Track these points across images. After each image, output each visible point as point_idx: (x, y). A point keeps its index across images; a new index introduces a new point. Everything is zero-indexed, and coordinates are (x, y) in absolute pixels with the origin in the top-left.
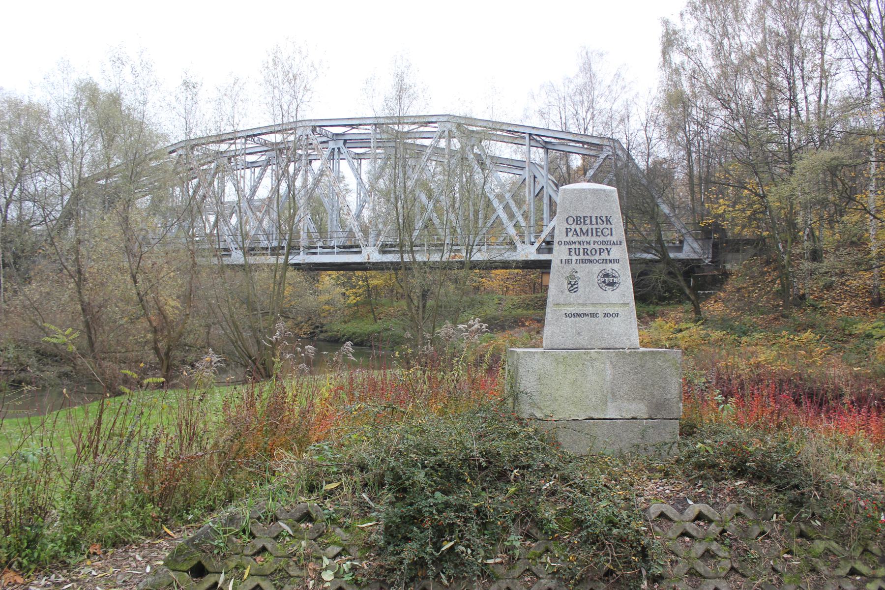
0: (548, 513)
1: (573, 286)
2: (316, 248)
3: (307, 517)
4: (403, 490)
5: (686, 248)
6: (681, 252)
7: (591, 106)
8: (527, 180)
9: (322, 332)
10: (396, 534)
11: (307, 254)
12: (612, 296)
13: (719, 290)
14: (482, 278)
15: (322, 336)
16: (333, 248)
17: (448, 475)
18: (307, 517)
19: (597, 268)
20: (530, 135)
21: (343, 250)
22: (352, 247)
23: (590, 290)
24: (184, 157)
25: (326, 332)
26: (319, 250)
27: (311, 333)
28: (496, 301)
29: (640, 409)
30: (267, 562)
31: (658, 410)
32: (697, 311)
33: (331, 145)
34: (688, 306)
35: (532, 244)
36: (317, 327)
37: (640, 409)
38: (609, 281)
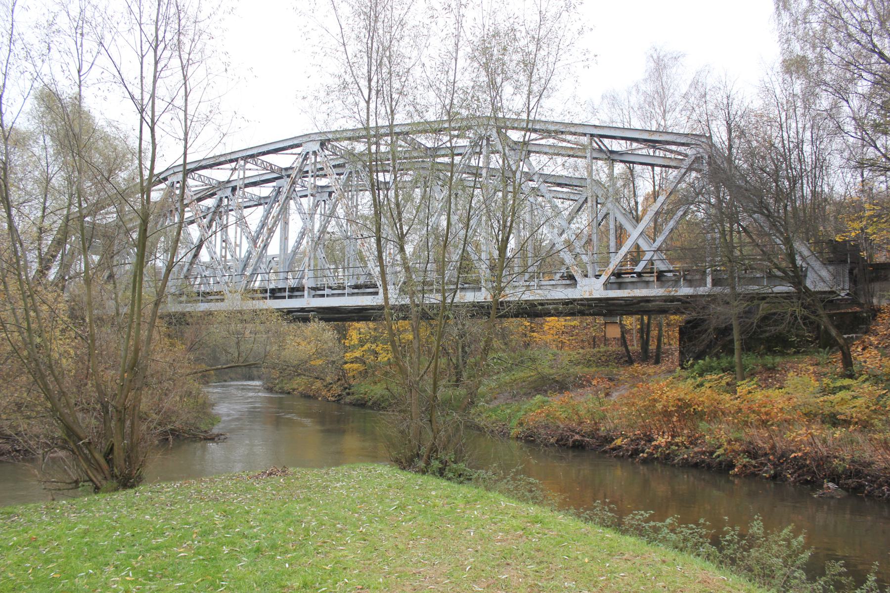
8: (589, 200)
9: (348, 394)
11: (314, 296)
13: (866, 333)
14: (534, 332)
15: (348, 399)
16: (344, 288)
21: (356, 291)
22: (367, 287)
27: (339, 395)
28: (550, 357)
32: (847, 361)
36: (346, 388)
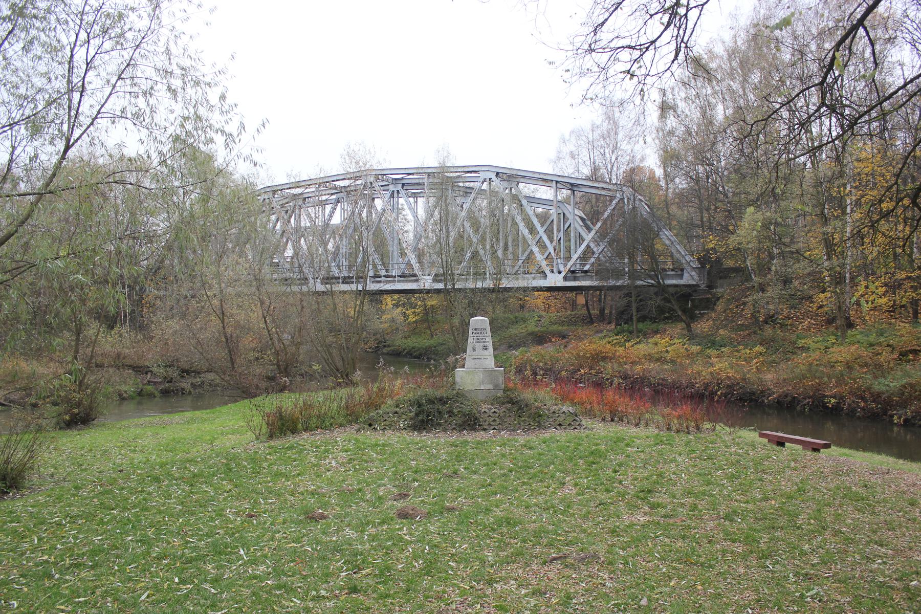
0: (455, 411)
1: (474, 350)
2: (380, 277)
3: (396, 413)
4: (420, 405)
5: (686, 275)
6: (682, 278)
7: (615, 148)
9: (385, 346)
10: (417, 415)
12: (486, 352)
15: (385, 350)
17: (431, 402)
18: (396, 413)
19: (481, 344)
20: (557, 182)
23: (479, 351)
24: (267, 201)
25: (389, 346)
26: (382, 279)
29: (491, 387)
30: (387, 423)
31: (496, 386)
33: (391, 188)
34: (679, 328)
35: (560, 272)
37: (491, 387)
38: (485, 348)
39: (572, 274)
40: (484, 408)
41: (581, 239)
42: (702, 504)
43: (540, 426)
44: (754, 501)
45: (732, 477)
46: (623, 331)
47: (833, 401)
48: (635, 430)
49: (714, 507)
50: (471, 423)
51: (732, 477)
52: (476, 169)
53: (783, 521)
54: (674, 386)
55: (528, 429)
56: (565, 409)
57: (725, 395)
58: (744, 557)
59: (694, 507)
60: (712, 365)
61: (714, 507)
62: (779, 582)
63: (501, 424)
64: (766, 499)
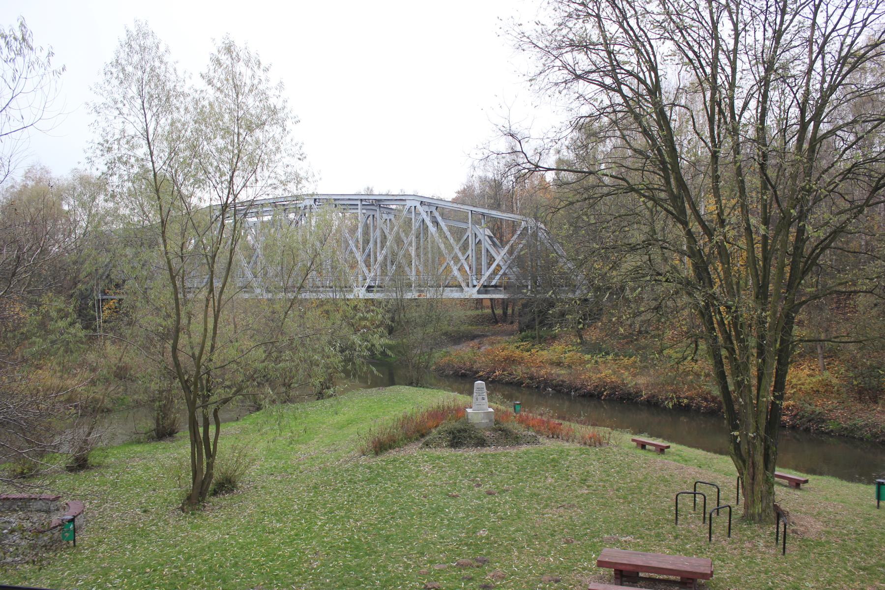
17: (459, 431)
31: (491, 421)
35: (474, 286)
37: (487, 421)
38: (483, 399)
39: (485, 289)
40: (487, 433)
41: (491, 259)
42: (607, 485)
43: (518, 444)
44: (627, 483)
45: (618, 472)
46: (527, 337)
47: (686, 401)
48: (567, 444)
49: (611, 486)
50: (481, 443)
51: (618, 472)
52: (403, 198)
53: (637, 491)
54: (571, 388)
55: (513, 446)
56: (530, 433)
57: (609, 395)
58: (623, 503)
59: (604, 486)
60: (600, 372)
61: (611, 486)
62: (634, 510)
63: (497, 443)
64: (632, 482)
